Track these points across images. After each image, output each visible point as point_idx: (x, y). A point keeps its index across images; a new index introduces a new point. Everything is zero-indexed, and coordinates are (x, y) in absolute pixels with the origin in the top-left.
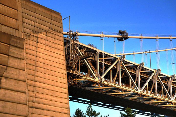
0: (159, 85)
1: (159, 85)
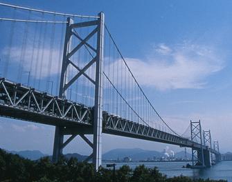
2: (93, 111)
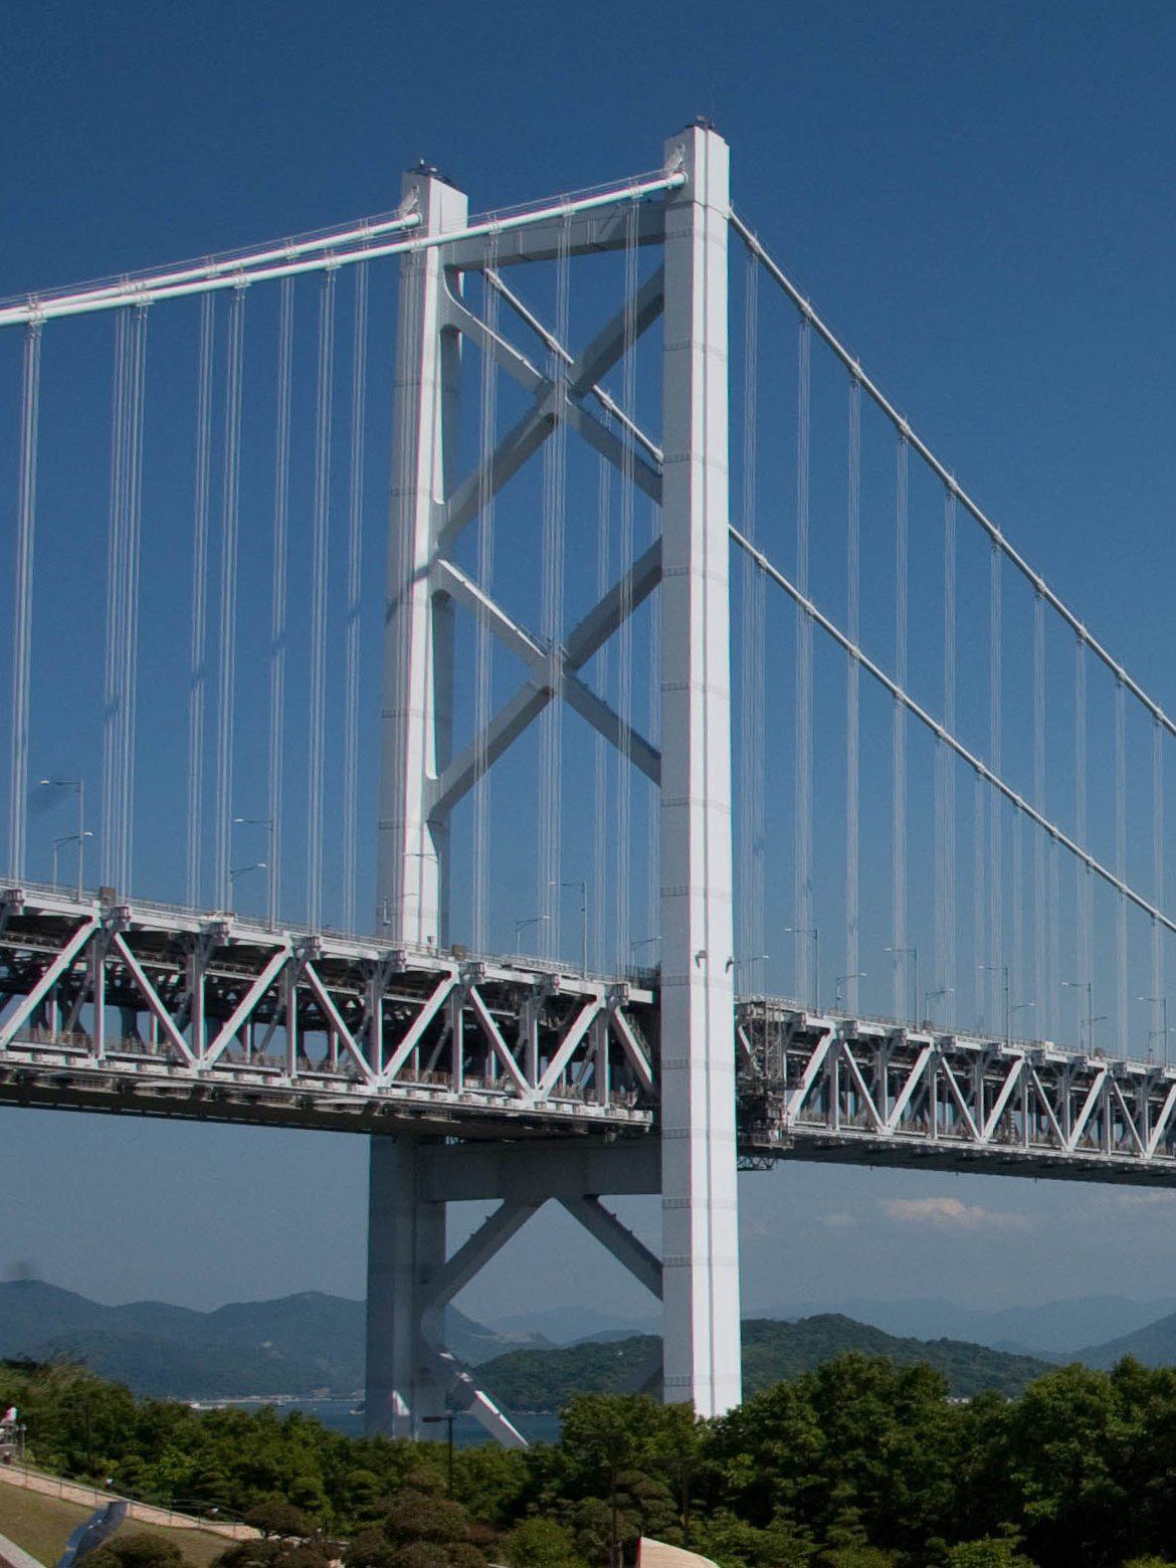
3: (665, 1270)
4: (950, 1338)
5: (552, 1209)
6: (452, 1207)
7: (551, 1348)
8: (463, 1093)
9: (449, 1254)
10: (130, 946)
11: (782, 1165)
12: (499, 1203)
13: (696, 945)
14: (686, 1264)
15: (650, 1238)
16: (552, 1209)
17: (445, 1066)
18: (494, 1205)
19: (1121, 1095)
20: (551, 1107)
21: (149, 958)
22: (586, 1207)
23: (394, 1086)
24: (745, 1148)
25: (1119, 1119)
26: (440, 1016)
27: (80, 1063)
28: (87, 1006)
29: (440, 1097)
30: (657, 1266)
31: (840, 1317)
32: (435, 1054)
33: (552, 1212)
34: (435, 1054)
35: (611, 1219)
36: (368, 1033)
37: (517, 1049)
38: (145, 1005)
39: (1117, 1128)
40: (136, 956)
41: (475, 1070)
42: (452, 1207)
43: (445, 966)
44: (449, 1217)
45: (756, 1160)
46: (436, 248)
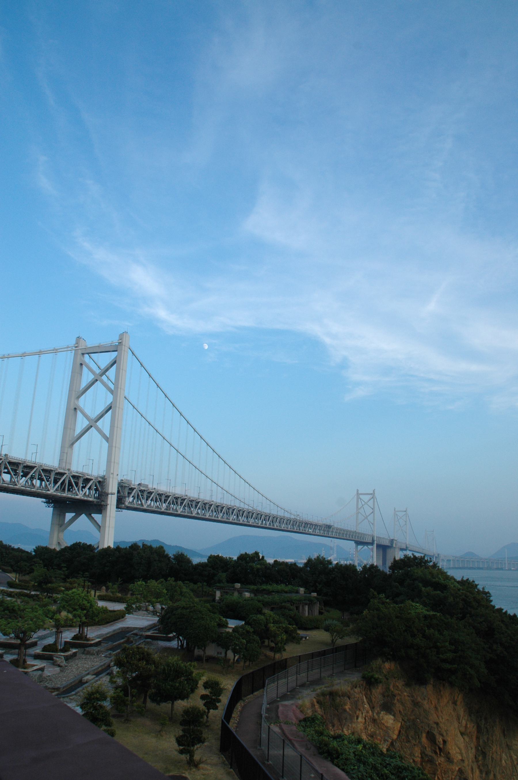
0: (70, 484)
1: (70, 484)
2: (101, 483)
3: (101, 528)
4: (177, 545)
5: (83, 515)
6: (67, 514)
7: (130, 545)
8: (66, 494)
9: (65, 522)
10: (9, 464)
11: (124, 510)
12: (74, 514)
13: (112, 471)
14: (105, 527)
15: (99, 522)
16: (83, 515)
17: (64, 490)
18: (73, 514)
19: (190, 503)
20: (83, 498)
21: (45, 473)
22: (89, 515)
23: (54, 492)
24: (118, 507)
25: (215, 512)
26: (64, 481)
27: (33, 490)
28: (35, 480)
29: (62, 494)
30: (100, 527)
31: (158, 540)
32: (62, 488)
33: (83, 516)
34: (62, 488)
35: (93, 518)
36: (79, 488)
37: (78, 487)
38: (44, 480)
39: (215, 513)
40: (10, 466)
41: (69, 490)
42: (67, 514)
43: (66, 472)
44: (66, 516)
45: (120, 510)
46: (87, 355)
